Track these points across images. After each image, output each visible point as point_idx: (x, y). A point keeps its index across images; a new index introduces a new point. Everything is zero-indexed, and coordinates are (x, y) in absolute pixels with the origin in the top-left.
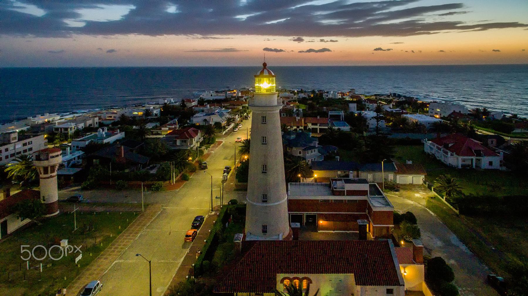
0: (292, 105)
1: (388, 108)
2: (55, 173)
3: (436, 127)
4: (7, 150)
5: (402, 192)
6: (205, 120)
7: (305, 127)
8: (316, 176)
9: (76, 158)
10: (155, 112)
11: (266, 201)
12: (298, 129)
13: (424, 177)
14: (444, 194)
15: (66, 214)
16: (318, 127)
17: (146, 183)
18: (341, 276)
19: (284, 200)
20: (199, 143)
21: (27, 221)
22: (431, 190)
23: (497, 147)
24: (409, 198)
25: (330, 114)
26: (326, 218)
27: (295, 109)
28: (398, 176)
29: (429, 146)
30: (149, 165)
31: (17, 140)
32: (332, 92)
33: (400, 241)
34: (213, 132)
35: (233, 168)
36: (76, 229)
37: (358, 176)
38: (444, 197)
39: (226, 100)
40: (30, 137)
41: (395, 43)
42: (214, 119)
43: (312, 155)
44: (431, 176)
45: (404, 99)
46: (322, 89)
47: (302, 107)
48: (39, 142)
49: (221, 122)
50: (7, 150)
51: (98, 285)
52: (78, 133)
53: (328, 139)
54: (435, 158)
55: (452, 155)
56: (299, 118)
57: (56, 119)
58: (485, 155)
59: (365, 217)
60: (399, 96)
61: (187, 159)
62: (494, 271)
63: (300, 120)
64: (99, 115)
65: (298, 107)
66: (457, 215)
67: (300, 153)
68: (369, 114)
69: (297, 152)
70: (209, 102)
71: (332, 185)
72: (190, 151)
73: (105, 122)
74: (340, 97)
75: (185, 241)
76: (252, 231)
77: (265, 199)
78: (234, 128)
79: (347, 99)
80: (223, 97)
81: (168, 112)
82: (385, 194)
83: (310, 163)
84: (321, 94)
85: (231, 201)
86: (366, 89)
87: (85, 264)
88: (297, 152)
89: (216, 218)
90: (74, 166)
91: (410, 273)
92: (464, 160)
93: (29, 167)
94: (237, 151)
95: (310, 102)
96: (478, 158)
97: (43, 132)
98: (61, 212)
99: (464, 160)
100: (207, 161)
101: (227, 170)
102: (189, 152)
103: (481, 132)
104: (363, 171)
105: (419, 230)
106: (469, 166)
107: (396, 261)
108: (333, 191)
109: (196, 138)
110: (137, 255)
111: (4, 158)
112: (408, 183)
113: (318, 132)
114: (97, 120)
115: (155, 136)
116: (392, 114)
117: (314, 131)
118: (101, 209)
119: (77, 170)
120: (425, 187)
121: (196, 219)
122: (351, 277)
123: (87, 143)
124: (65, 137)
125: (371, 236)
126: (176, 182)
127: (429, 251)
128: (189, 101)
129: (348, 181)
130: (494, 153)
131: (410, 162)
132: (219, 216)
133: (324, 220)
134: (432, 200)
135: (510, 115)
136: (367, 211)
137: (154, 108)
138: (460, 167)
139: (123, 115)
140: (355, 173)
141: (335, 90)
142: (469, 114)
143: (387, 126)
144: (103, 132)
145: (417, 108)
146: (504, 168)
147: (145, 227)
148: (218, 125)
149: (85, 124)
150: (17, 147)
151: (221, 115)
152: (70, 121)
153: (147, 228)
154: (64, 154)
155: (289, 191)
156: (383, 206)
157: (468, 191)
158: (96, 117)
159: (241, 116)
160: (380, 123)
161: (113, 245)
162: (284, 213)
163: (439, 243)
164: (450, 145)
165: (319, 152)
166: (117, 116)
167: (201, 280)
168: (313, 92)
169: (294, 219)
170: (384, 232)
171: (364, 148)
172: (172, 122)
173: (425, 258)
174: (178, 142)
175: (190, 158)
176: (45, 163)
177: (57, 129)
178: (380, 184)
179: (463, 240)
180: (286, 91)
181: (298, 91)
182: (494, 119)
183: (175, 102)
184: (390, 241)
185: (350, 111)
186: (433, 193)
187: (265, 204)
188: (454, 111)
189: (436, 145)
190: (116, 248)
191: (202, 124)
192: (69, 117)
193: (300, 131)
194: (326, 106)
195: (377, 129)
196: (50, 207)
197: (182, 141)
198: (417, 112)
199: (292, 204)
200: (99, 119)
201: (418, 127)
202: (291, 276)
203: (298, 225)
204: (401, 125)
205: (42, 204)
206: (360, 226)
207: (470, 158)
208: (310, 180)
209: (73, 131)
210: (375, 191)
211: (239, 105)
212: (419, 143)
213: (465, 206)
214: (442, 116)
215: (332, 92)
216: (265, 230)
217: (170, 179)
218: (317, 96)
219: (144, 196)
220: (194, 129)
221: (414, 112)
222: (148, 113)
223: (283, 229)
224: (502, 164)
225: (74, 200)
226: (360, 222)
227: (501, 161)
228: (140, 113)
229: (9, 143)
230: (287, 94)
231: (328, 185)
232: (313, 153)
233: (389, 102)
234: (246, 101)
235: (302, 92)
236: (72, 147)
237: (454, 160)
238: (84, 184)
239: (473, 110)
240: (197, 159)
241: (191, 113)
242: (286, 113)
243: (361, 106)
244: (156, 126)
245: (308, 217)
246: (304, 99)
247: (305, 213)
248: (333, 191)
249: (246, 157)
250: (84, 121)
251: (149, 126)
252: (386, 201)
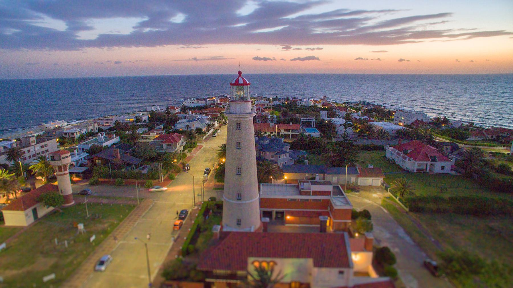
0: (267, 112)
1: (356, 115)
2: (68, 171)
3: (400, 135)
4: (29, 151)
5: (362, 192)
6: (187, 126)
7: (278, 133)
8: (286, 177)
9: (83, 159)
10: (144, 118)
11: (240, 199)
12: (272, 135)
13: (382, 179)
14: (398, 194)
15: (79, 204)
16: (290, 133)
17: (139, 181)
18: (302, 261)
19: (256, 199)
20: (182, 147)
21: (51, 208)
22: (387, 191)
23: (451, 153)
24: (367, 198)
25: (302, 120)
26: (292, 214)
27: (270, 116)
28: (359, 179)
29: (390, 152)
30: (141, 165)
31: (35, 143)
32: (305, 100)
33: (355, 232)
34: (194, 137)
35: (212, 169)
36: (88, 216)
37: (324, 178)
38: (398, 198)
39: (206, 107)
40: (45, 141)
41: (409, 10)
42: (195, 125)
43: (284, 159)
44: (388, 179)
45: (372, 107)
46: (296, 96)
47: (277, 114)
48: (53, 145)
49: (201, 128)
50: (29, 151)
51: (109, 259)
52: (82, 138)
53: (300, 145)
54: (394, 163)
55: (409, 160)
56: (273, 124)
57: (64, 124)
58: (439, 161)
59: (328, 214)
60: (368, 104)
61: (173, 161)
62: (431, 258)
63: (274, 127)
64: (98, 121)
65: (272, 113)
66: (407, 213)
67: (272, 157)
68: (339, 121)
69: (269, 156)
70: (190, 109)
71: (300, 186)
72: (174, 154)
73: (103, 128)
74: (313, 104)
75: (174, 228)
76: (228, 224)
77: (239, 197)
78: (213, 133)
79: (319, 106)
80: (203, 105)
81: (155, 119)
82: (346, 194)
83: (281, 166)
84: (295, 102)
85: (210, 198)
86: (337, 98)
87: (98, 242)
88: (269, 156)
89: (198, 211)
90: (82, 165)
91: (360, 259)
92: (419, 165)
93: (47, 165)
94: (216, 155)
95: (284, 109)
96: (432, 163)
97: (55, 136)
98: (76, 202)
99: (419, 165)
100: (189, 163)
101: (208, 171)
102: (175, 155)
103: (438, 139)
104: (329, 174)
105: (372, 225)
106: (423, 170)
107: (348, 248)
108: (300, 191)
109: (180, 143)
110: (136, 238)
111: (27, 158)
112: (368, 185)
113: (290, 137)
114: (96, 125)
115: (144, 141)
116: (360, 121)
117: (287, 136)
118: (105, 201)
119: (84, 169)
120: (382, 188)
121: (182, 212)
122: (310, 262)
123: (90, 146)
124: (73, 141)
125: (330, 229)
126: (164, 180)
127: (379, 241)
128: (173, 108)
129: (316, 183)
130: (446, 158)
131: (372, 167)
132: (200, 210)
133: (291, 215)
134: (388, 200)
135: (468, 124)
136: (329, 209)
137: (143, 115)
138: (415, 171)
139: (117, 121)
140: (322, 175)
141: (309, 96)
142: (430, 123)
143: (354, 133)
144: (101, 137)
145: (383, 116)
146: (454, 173)
147: (141, 217)
148: (199, 131)
149: (87, 130)
150: (36, 149)
151: (202, 121)
152: (75, 127)
153: (143, 217)
154: (72, 155)
155: (261, 191)
156: (342, 204)
157: (420, 191)
158: (95, 123)
159: (220, 123)
160: (347, 129)
161: (118, 229)
162: (257, 211)
163: (388, 235)
164: (409, 151)
165: (290, 156)
166: (113, 122)
167: (188, 259)
168: (287, 99)
169: (266, 214)
170: (343, 226)
171: (331, 154)
172: (159, 127)
173: (374, 247)
174: (165, 146)
175: (175, 161)
176: (59, 163)
177: (66, 134)
178: (343, 186)
179: (409, 234)
180: (261, 98)
181: (273, 99)
182: (452, 127)
183: (161, 109)
184: (346, 234)
185: (322, 118)
186: (389, 194)
187: (239, 202)
188: (417, 119)
189: (397, 151)
190: (120, 232)
191: (184, 129)
192: (74, 123)
193: (274, 137)
194: (299, 113)
195: (345, 136)
196: (66, 199)
197: (168, 145)
198: (383, 120)
199: (263, 202)
200: (99, 125)
201: (382, 134)
202: (261, 259)
203: (267, 219)
204: (367, 131)
205: (60, 196)
206: (321, 221)
207: (425, 163)
208: (280, 181)
209: (78, 135)
210: (338, 191)
211: (219, 112)
212: (381, 149)
213: (416, 206)
214: (405, 124)
215: (305, 100)
216: (239, 223)
217: (159, 178)
218: (291, 103)
219: (138, 192)
220: (178, 134)
221: (381, 120)
222: (137, 119)
223: (255, 222)
224: (453, 168)
225: (84, 193)
226: (321, 218)
227: (452, 166)
228: (132, 120)
229: (29, 145)
230: (262, 101)
231: (296, 186)
232: (285, 157)
233: (359, 109)
234: (224, 108)
235: (276, 99)
236: (79, 150)
237: (411, 165)
238: (92, 180)
239: (435, 118)
240: (181, 161)
241: (174, 120)
242: (260, 120)
243: (332, 113)
244: (146, 132)
245: (277, 213)
246: (279, 106)
247: (275, 210)
248: (300, 191)
249: (224, 160)
250: (86, 127)
251: (140, 131)
252: (347, 201)
